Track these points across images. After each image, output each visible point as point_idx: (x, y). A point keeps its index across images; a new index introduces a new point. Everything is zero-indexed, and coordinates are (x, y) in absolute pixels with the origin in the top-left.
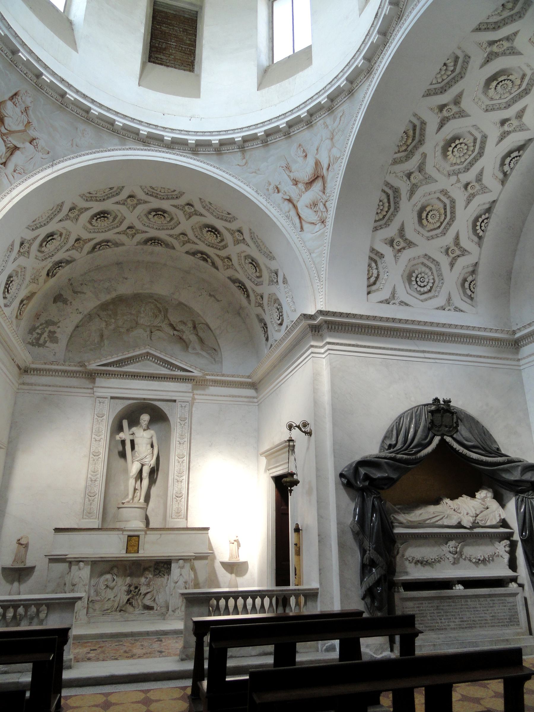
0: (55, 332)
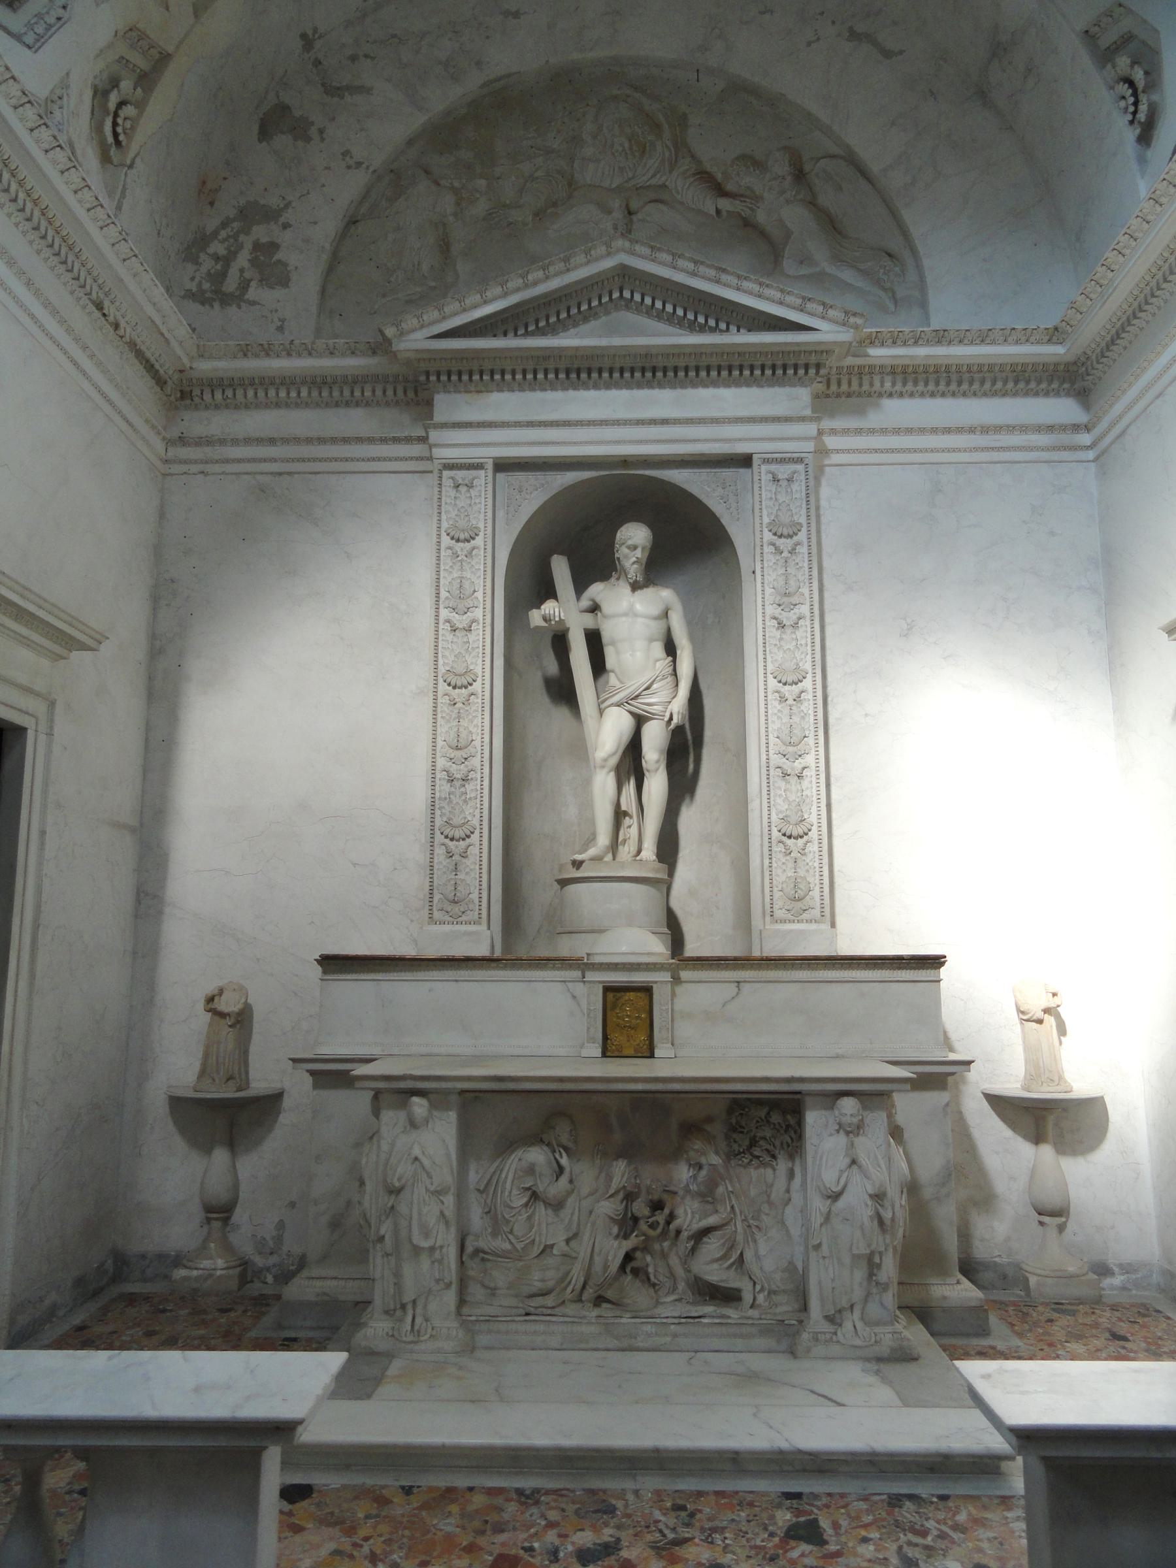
0: (273, 247)
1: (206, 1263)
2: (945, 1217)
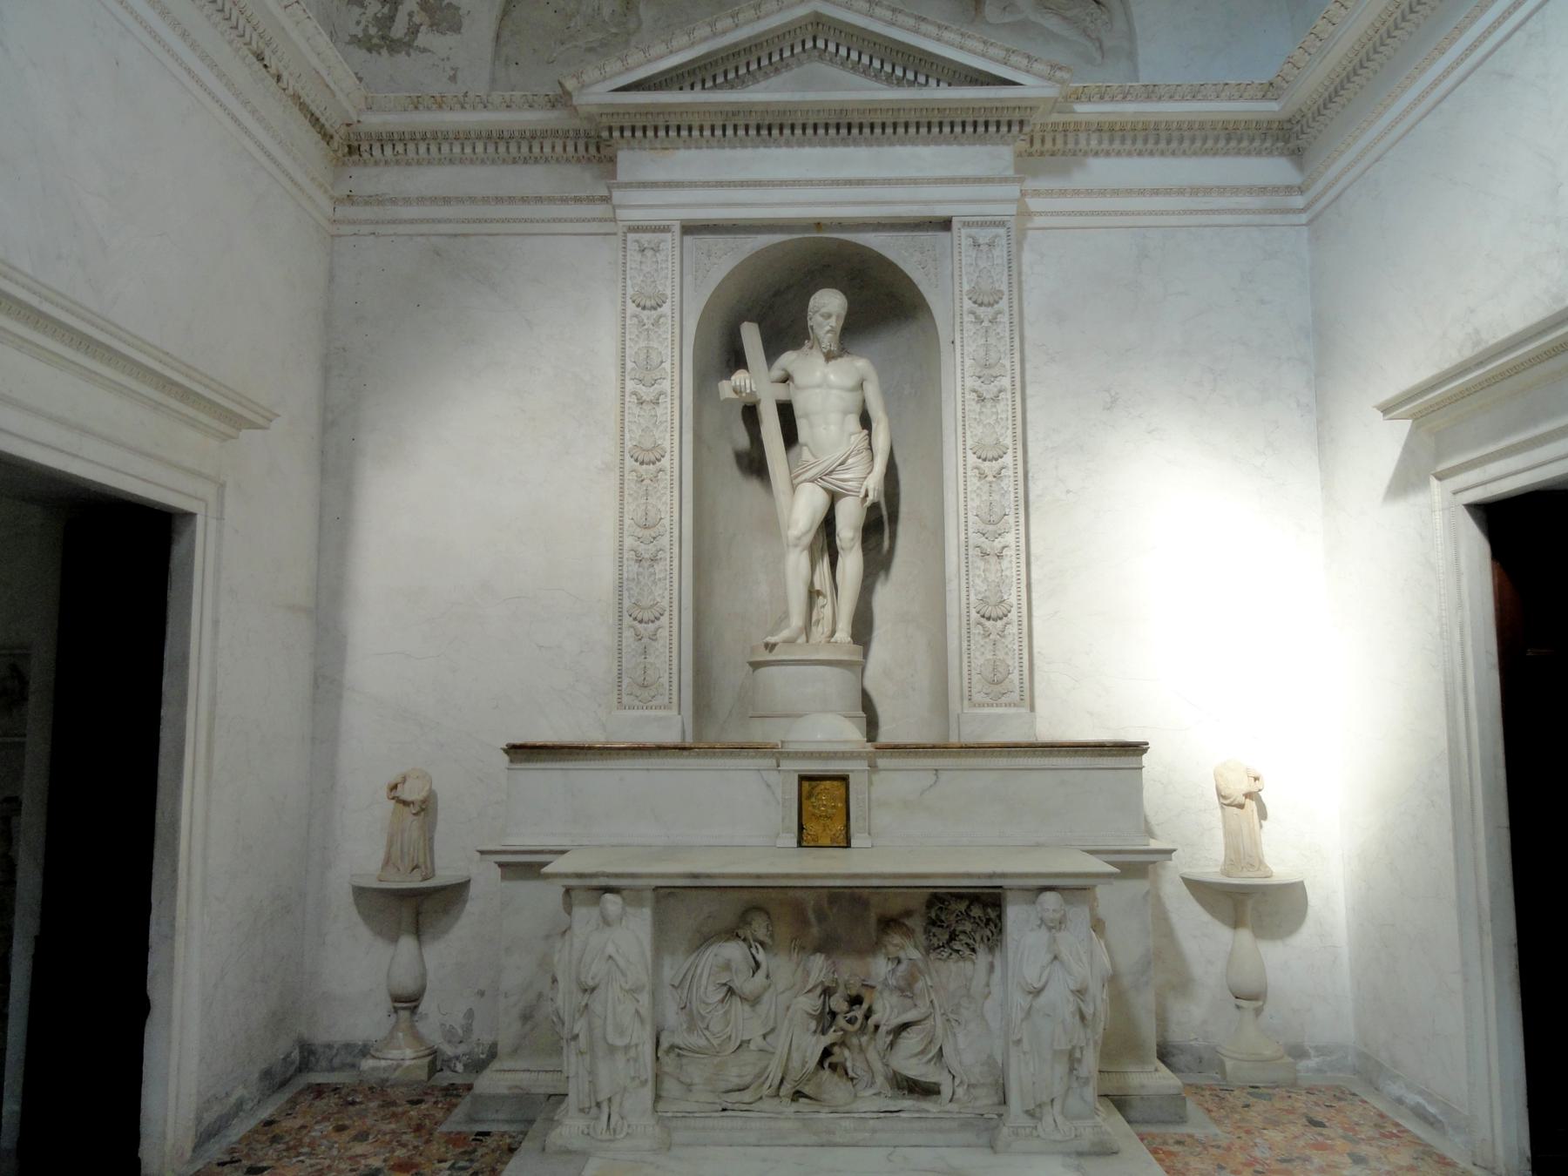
1: (395, 1054)
2: (1143, 1005)
